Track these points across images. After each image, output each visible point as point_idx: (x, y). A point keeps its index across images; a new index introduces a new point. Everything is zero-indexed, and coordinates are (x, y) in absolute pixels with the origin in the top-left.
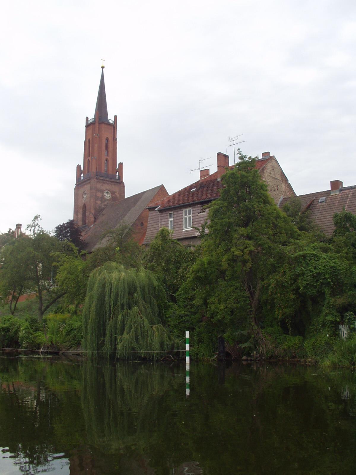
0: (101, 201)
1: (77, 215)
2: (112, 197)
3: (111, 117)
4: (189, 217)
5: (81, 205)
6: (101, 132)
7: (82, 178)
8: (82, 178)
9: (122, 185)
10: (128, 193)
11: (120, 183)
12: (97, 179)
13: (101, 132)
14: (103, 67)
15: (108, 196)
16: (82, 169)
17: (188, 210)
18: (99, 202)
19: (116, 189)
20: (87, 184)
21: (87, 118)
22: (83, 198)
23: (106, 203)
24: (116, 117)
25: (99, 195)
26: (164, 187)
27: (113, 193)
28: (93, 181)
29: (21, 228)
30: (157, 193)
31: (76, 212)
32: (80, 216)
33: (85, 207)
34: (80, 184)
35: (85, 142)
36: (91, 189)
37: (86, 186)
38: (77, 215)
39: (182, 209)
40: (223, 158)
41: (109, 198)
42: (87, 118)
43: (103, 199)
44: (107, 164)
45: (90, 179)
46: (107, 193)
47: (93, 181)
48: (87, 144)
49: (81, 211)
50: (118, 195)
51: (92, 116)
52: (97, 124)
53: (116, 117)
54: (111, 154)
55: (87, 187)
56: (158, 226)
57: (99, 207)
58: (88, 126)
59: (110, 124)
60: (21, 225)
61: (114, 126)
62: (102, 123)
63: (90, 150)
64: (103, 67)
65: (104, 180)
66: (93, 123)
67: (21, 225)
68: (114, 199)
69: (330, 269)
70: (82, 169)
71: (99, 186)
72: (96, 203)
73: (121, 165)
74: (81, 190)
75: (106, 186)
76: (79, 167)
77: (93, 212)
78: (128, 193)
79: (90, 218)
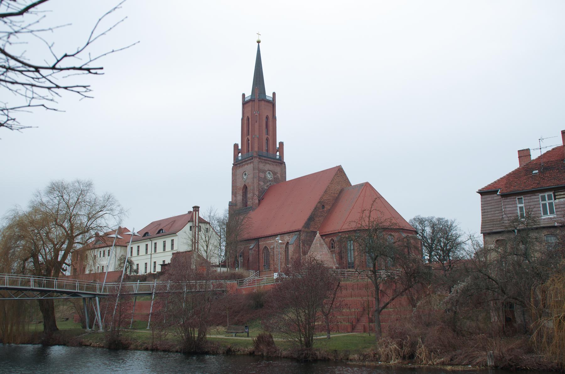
0: (264, 182)
1: (236, 196)
2: (274, 178)
3: (269, 94)
4: (545, 200)
5: (240, 185)
6: (259, 110)
7: (240, 158)
8: (240, 158)
9: (283, 165)
10: (290, 175)
11: (281, 163)
12: (259, 159)
13: (259, 110)
14: (259, 42)
15: (269, 177)
16: (240, 147)
17: (546, 194)
18: (262, 183)
19: (278, 169)
20: (247, 164)
21: (244, 95)
22: (243, 178)
23: (268, 184)
24: (274, 94)
25: (262, 175)
26: (342, 169)
27: (275, 173)
28: (256, 160)
29: (198, 211)
30: (336, 175)
31: (234, 193)
32: (240, 198)
33: (245, 187)
34: (237, 164)
35: (242, 119)
36: (254, 169)
37: (246, 166)
38: (236, 196)
39: (537, 194)
40: (524, 154)
41: (271, 179)
42: (244, 95)
43: (265, 180)
44: (267, 143)
45: (252, 159)
46: (269, 173)
47: (256, 160)
48: (245, 122)
49: (241, 192)
50: (279, 176)
51: (248, 94)
52: (256, 101)
53: (274, 94)
54: (271, 133)
55: (248, 168)
56: (500, 206)
57: (262, 189)
58: (245, 103)
59: (268, 101)
60: (199, 207)
61: (272, 103)
62: (262, 100)
63: (249, 128)
64: (259, 42)
65: (266, 160)
66: (252, 100)
67: (199, 207)
68: (276, 180)
69: (439, 251)
70: (240, 147)
71: (261, 166)
72: (259, 184)
73: (281, 144)
74: (240, 171)
75: (268, 167)
76: (236, 146)
77: (257, 193)
78: (290, 175)
79: (252, 199)
